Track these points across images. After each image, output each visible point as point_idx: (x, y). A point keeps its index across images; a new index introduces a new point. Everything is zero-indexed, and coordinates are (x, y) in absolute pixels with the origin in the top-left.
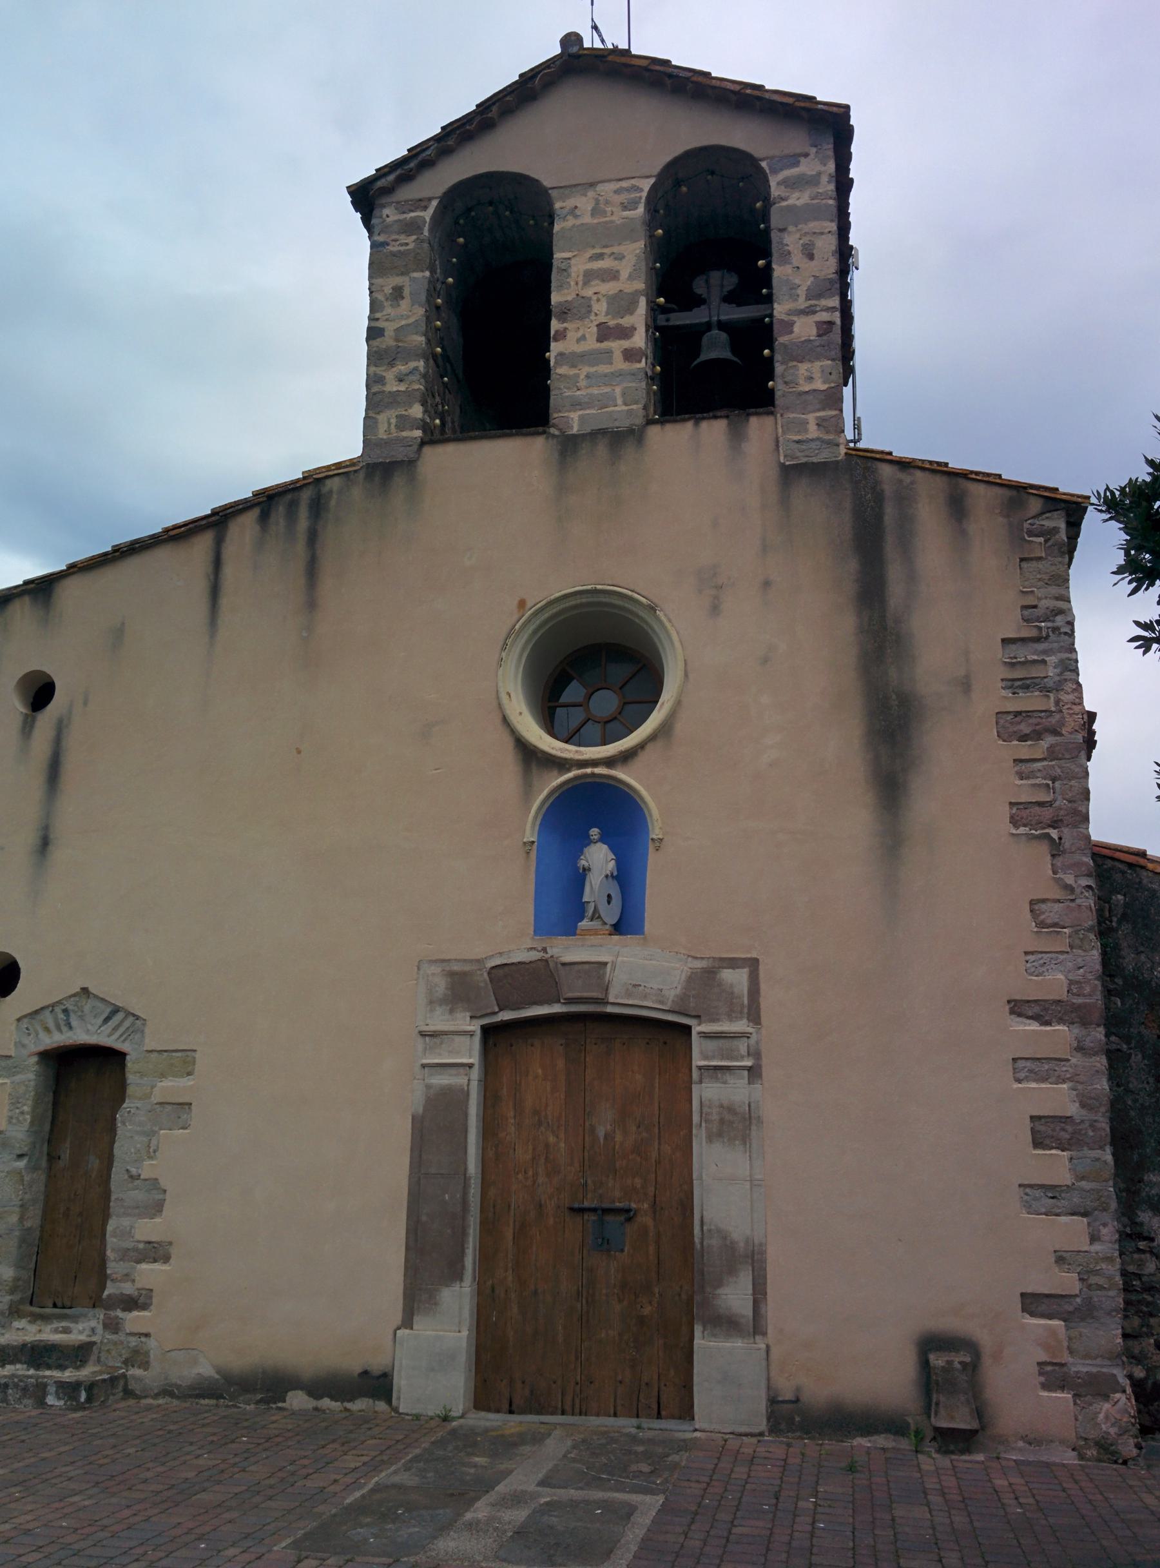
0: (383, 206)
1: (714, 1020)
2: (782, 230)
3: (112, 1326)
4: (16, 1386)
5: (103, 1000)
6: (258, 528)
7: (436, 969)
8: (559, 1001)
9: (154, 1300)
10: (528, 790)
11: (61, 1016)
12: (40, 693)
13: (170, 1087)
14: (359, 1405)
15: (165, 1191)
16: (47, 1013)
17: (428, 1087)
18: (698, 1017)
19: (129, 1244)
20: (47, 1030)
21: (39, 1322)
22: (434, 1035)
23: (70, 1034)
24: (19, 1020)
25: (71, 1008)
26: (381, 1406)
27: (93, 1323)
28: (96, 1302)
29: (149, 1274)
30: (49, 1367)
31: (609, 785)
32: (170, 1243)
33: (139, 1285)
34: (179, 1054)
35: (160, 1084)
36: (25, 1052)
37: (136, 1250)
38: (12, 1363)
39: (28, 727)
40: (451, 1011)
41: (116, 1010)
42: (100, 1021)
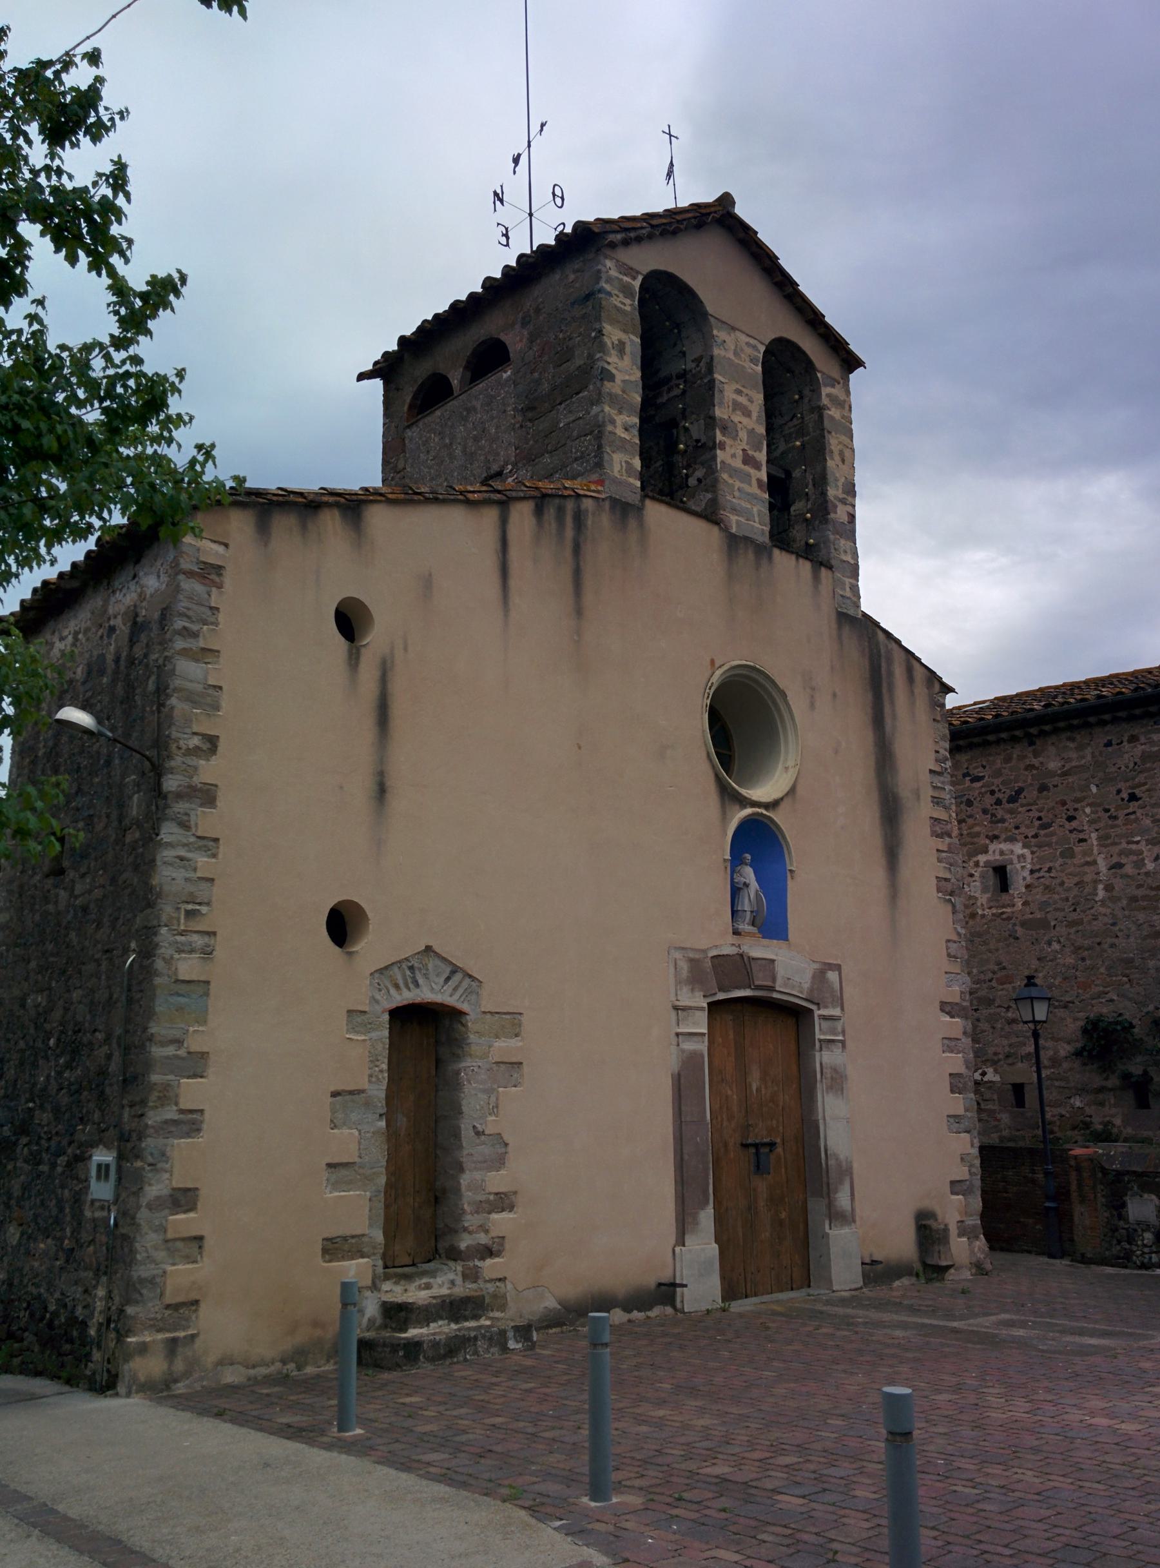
0: (606, 257)
1: (826, 1007)
2: (829, 432)
3: (471, 1275)
4: (484, 1336)
5: (444, 960)
6: (533, 520)
7: (678, 955)
8: (750, 987)
9: (507, 1246)
10: (724, 818)
11: (408, 973)
12: (349, 621)
13: (504, 1047)
14: (655, 1312)
15: (506, 1145)
16: (396, 969)
17: (683, 1051)
18: (818, 1004)
19: (481, 1197)
20: (397, 986)
21: (402, 1282)
22: (685, 1009)
23: (417, 991)
24: (371, 974)
25: (416, 965)
26: (669, 1310)
27: (451, 1276)
28: (454, 1255)
29: (501, 1221)
30: (466, 1319)
31: (762, 822)
32: (515, 1193)
33: (493, 1234)
34: (508, 1017)
35: (496, 1044)
36: (378, 1008)
37: (488, 1201)
38: (435, 1321)
39: (354, 659)
40: (692, 990)
41: (455, 970)
42: (442, 980)
